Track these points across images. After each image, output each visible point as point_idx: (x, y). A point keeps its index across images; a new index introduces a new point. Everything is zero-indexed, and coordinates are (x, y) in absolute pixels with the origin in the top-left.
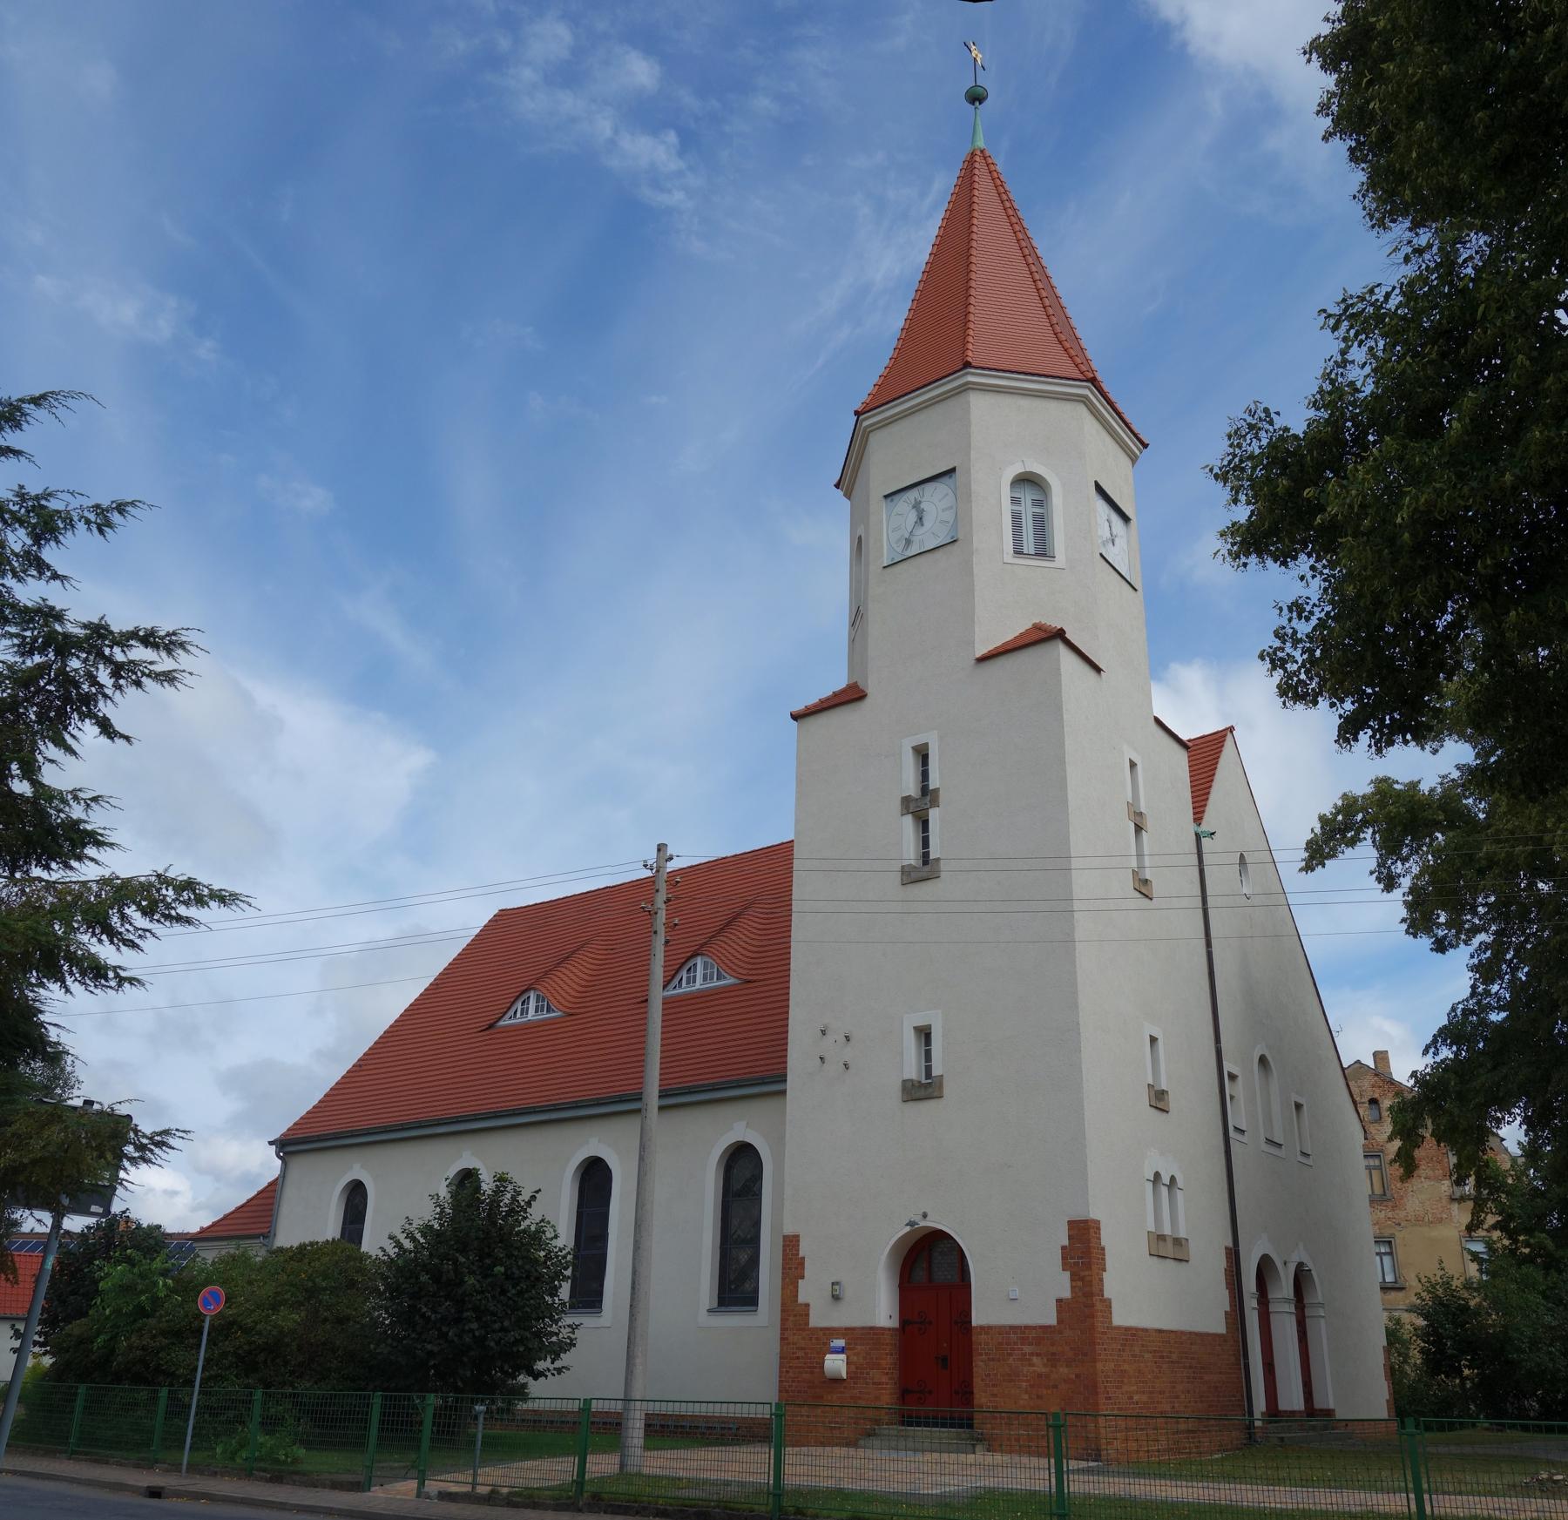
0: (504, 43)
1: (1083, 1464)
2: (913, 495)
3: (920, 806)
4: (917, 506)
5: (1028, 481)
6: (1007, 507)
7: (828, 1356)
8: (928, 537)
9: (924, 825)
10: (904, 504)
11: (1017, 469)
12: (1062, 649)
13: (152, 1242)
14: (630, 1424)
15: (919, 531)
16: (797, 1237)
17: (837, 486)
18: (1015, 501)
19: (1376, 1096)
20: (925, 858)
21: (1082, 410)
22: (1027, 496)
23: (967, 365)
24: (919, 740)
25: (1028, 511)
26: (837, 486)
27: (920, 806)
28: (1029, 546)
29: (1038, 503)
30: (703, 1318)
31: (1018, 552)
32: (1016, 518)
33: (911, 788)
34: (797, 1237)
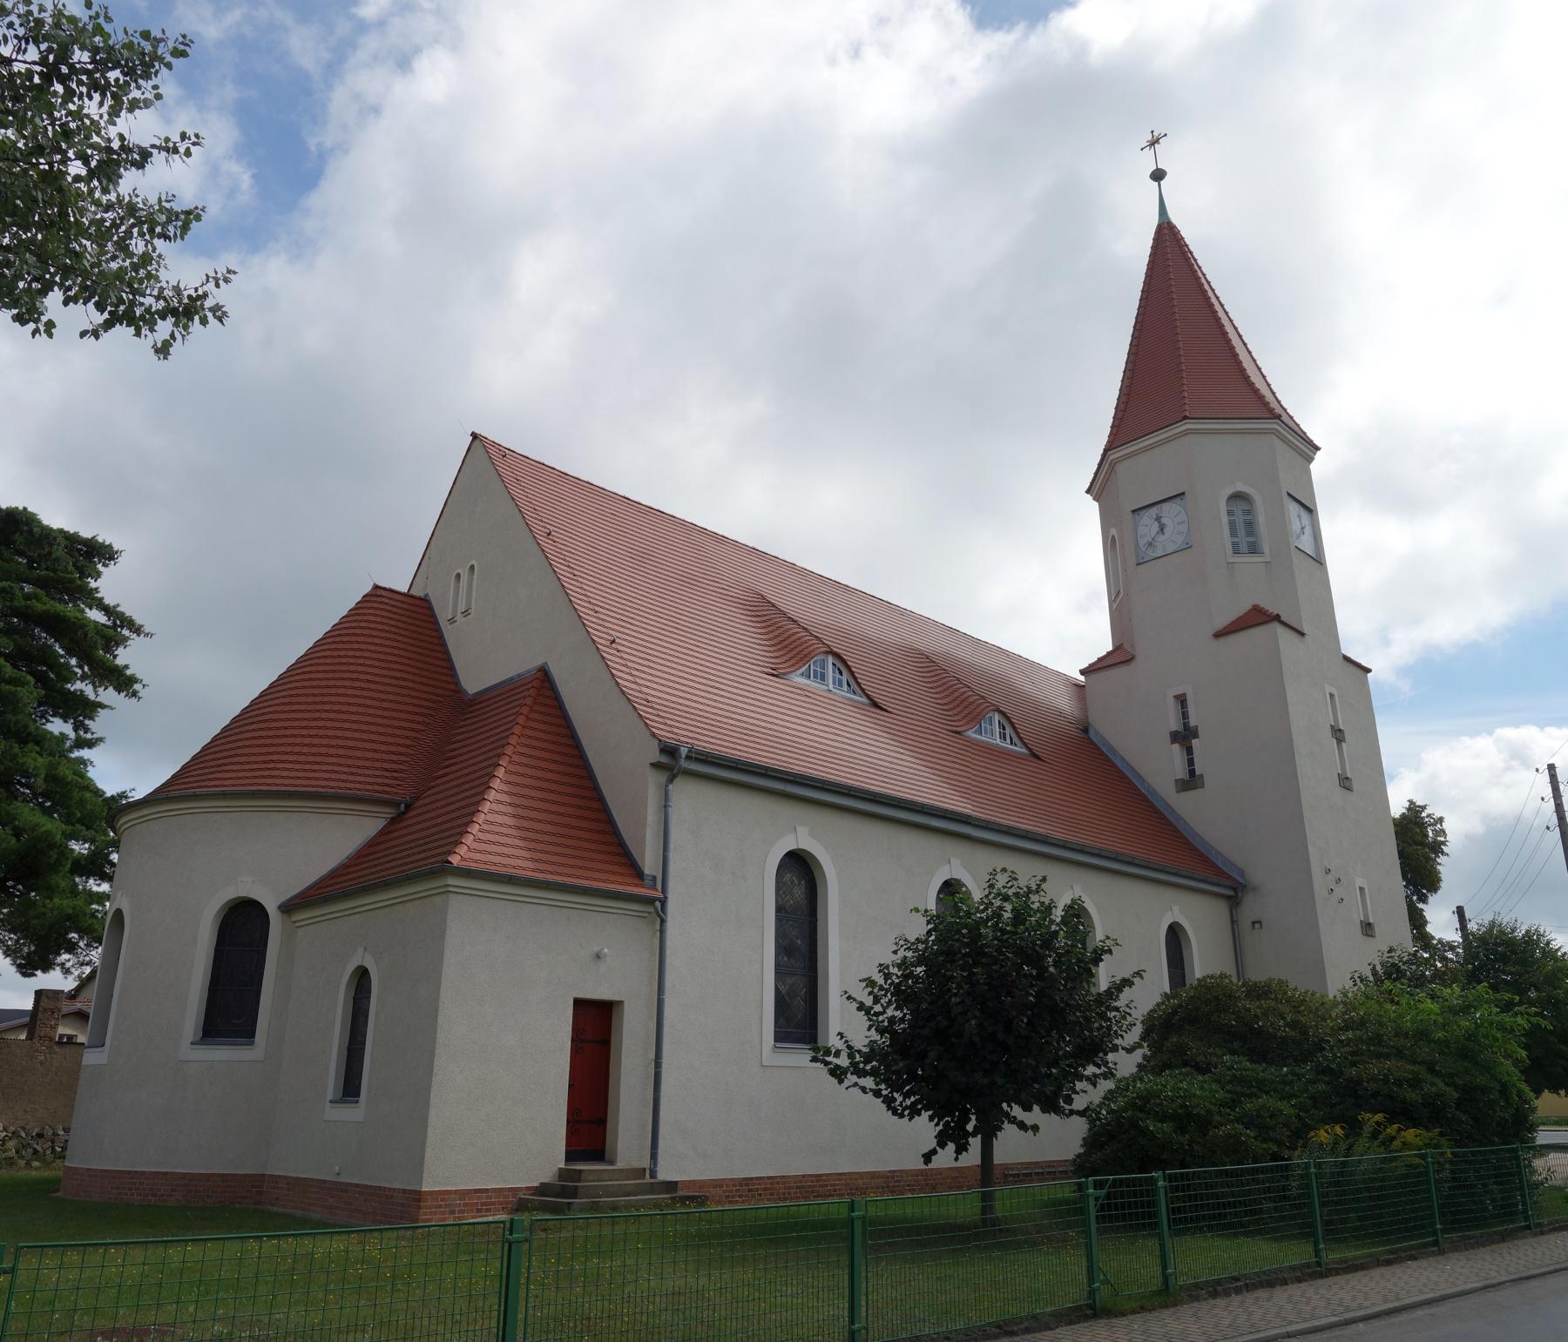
2: (1154, 511)
3: (1185, 736)
4: (1158, 519)
5: (1237, 497)
6: (1225, 519)
8: (1167, 543)
9: (1189, 751)
10: (1147, 518)
11: (1230, 491)
12: (1280, 629)
14: (74, 1257)
15: (1161, 538)
16: (579, 1004)
17: (1088, 492)
18: (1230, 513)
19: (596, 949)
20: (1192, 773)
22: (1239, 507)
23: (1185, 418)
25: (1240, 518)
26: (1088, 492)
27: (1185, 736)
28: (1244, 547)
31: (1236, 551)
32: (1232, 525)
34: (579, 1004)
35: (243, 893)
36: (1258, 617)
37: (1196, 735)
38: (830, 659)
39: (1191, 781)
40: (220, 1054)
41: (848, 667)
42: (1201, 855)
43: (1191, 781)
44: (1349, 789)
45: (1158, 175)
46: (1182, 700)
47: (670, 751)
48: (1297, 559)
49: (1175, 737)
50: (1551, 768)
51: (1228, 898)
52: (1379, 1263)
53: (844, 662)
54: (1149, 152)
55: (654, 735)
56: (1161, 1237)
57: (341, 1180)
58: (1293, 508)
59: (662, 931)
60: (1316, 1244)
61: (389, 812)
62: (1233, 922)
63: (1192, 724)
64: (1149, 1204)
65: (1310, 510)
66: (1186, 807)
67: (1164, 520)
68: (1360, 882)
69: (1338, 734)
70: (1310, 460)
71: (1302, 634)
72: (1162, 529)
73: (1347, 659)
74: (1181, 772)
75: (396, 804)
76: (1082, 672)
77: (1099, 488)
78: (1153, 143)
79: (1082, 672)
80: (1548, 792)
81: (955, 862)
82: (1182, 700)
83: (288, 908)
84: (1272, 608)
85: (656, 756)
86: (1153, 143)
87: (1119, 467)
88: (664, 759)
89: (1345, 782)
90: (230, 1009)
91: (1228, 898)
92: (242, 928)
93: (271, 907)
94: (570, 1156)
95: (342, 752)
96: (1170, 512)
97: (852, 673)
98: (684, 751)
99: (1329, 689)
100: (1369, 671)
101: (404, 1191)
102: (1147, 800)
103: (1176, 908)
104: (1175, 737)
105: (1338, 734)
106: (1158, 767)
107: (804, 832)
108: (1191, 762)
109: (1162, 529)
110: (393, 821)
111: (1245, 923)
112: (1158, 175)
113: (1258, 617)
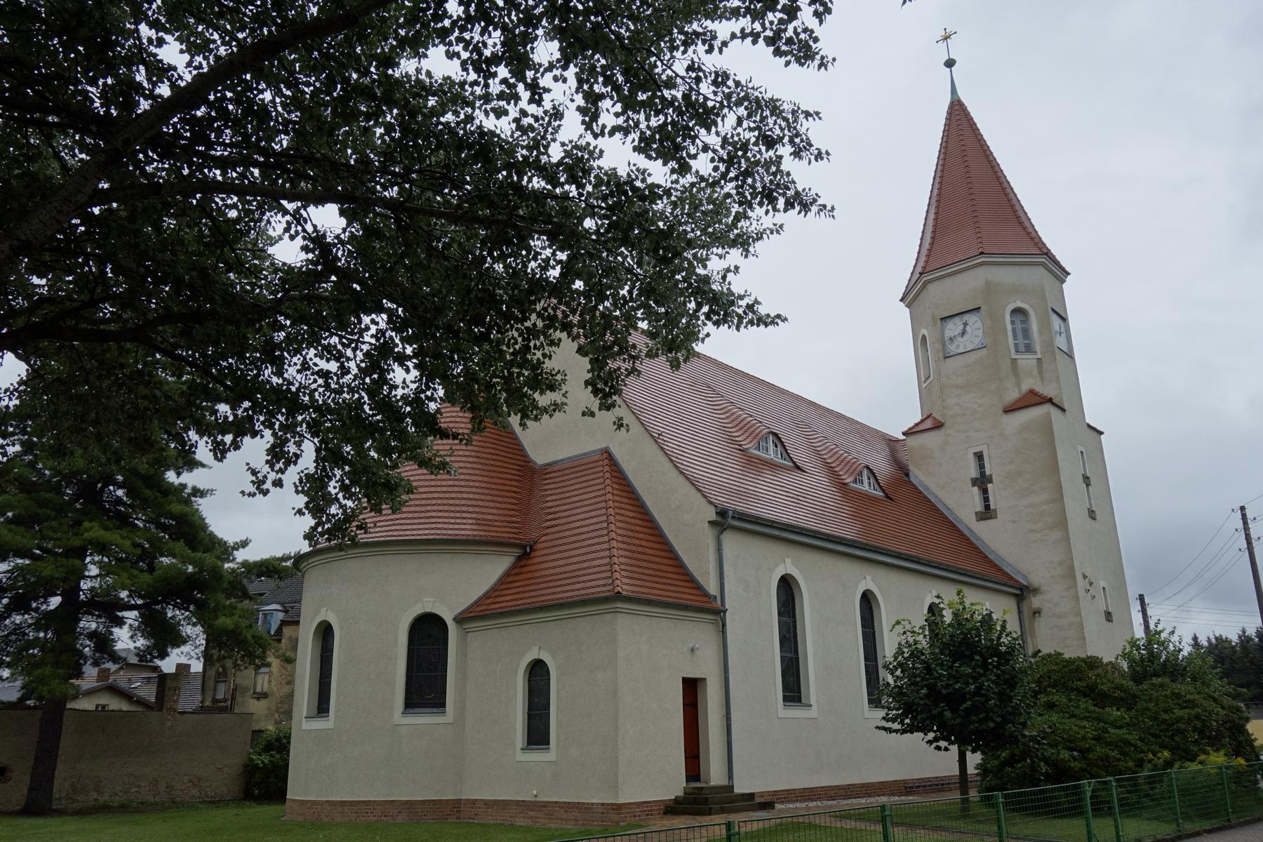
0: (781, 203)
1: (801, 820)
5: (1018, 311)
6: (1009, 327)
7: (954, 749)
13: (259, 651)
15: (960, 339)
17: (902, 300)
18: (1013, 323)
20: (987, 507)
21: (1041, 269)
22: (1019, 318)
24: (977, 449)
26: (902, 300)
27: (982, 482)
28: (1022, 348)
29: (1023, 322)
30: (813, 712)
31: (1017, 351)
32: (1014, 330)
33: (974, 473)
35: (428, 610)
36: (1033, 399)
37: (991, 481)
38: (771, 437)
39: (987, 513)
40: (423, 720)
41: (782, 443)
42: (995, 565)
43: (987, 513)
44: (1094, 519)
45: (950, 63)
46: (979, 457)
47: (722, 513)
48: (1059, 355)
49: (975, 482)
50: (1243, 508)
51: (1016, 595)
52: (1209, 832)
53: (779, 439)
54: (943, 45)
55: (711, 503)
56: (1087, 819)
57: (538, 799)
58: (1054, 317)
59: (724, 632)
60: (1115, 821)
61: (518, 552)
62: (1020, 612)
63: (988, 473)
64: (1108, 802)
65: (1064, 319)
66: (984, 532)
67: (968, 328)
68: (1102, 584)
69: (1086, 480)
70: (1063, 281)
71: (1063, 410)
72: (963, 333)
73: (1089, 426)
74: (979, 507)
75: (524, 547)
76: (904, 434)
77: (910, 297)
78: (946, 38)
79: (904, 434)
80: (1240, 525)
81: (788, 561)
82: (979, 457)
83: (460, 620)
84: (1047, 391)
85: (713, 517)
86: (946, 38)
87: (930, 287)
88: (719, 519)
89: (1092, 514)
90: (425, 685)
91: (1016, 595)
92: (427, 635)
93: (449, 619)
94: (688, 780)
95: (446, 508)
96: (972, 319)
97: (784, 446)
98: (730, 513)
99: (1080, 448)
100: (1101, 433)
101: (603, 804)
102: (955, 526)
103: (788, 561)
104: (975, 482)
105: (1086, 480)
106: (962, 504)
107: (789, 563)
108: (986, 500)
109: (963, 333)
110: (519, 558)
111: (1026, 613)
112: (950, 63)
113: (1033, 399)
